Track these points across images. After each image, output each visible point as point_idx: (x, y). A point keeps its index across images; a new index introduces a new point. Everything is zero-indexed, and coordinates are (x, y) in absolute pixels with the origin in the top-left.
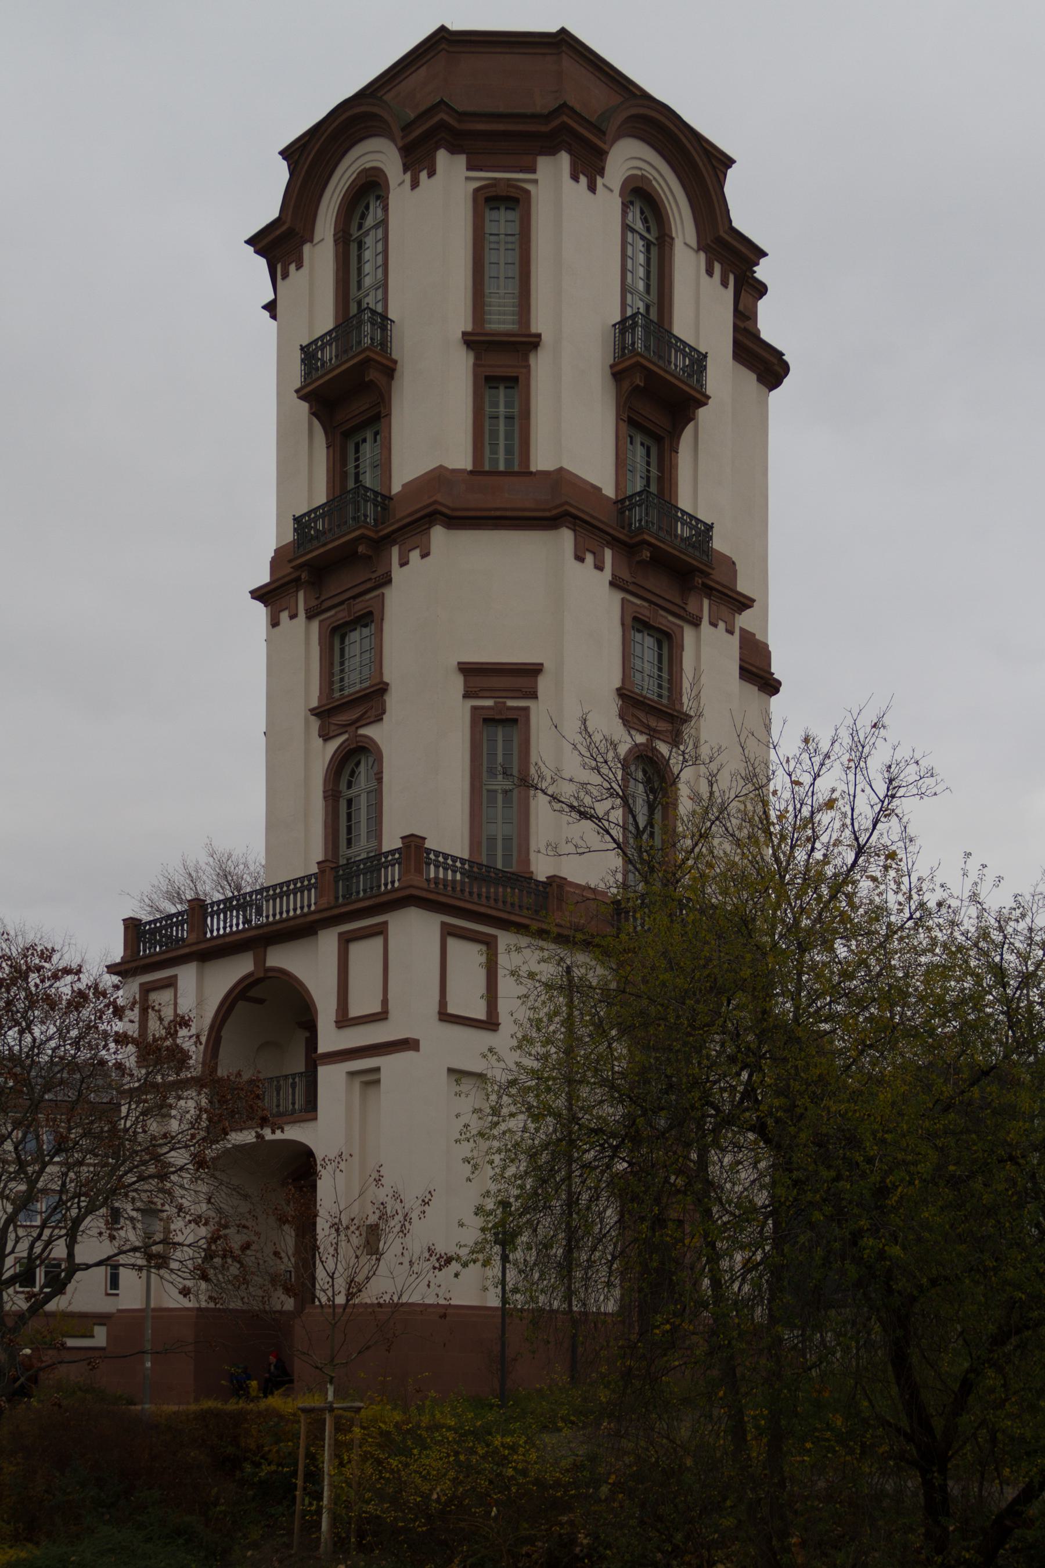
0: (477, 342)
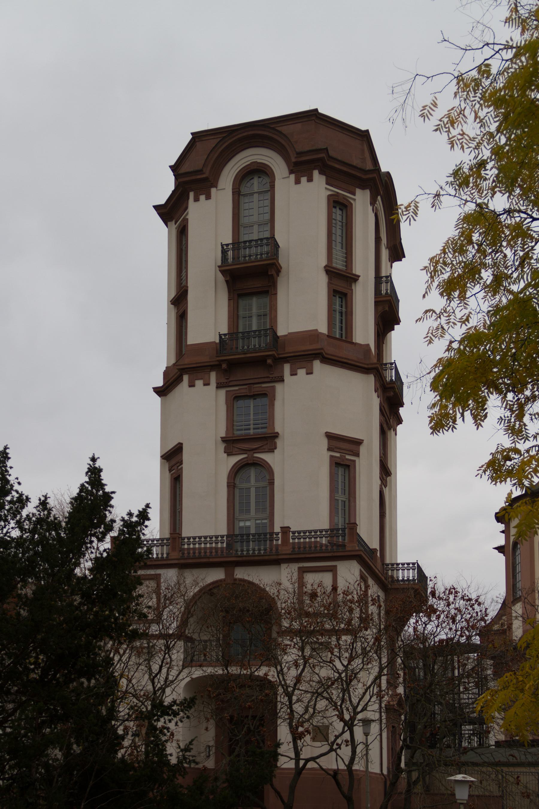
0: (330, 272)
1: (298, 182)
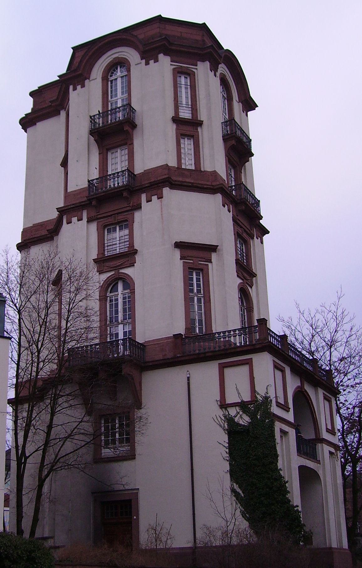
1: (147, 64)
